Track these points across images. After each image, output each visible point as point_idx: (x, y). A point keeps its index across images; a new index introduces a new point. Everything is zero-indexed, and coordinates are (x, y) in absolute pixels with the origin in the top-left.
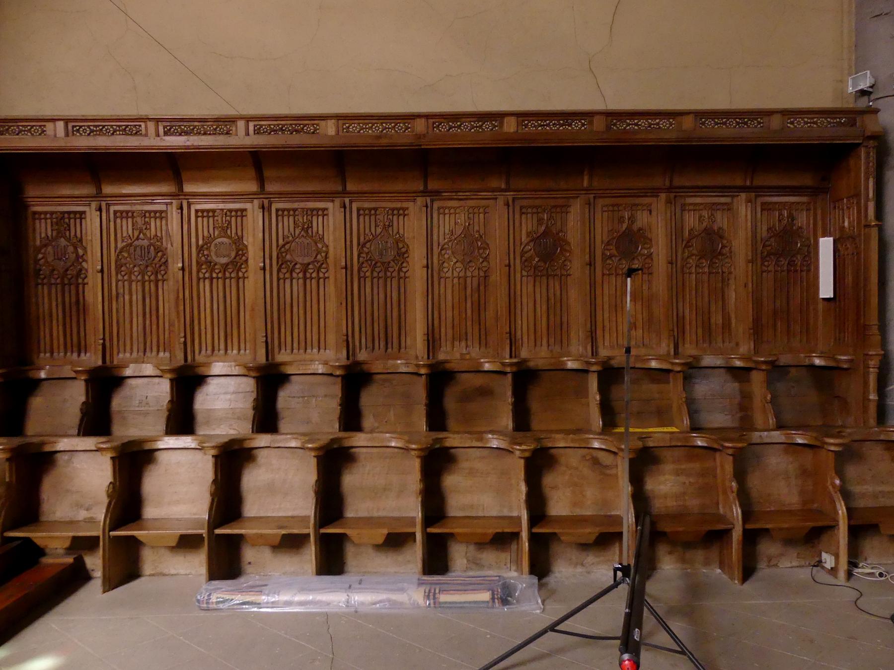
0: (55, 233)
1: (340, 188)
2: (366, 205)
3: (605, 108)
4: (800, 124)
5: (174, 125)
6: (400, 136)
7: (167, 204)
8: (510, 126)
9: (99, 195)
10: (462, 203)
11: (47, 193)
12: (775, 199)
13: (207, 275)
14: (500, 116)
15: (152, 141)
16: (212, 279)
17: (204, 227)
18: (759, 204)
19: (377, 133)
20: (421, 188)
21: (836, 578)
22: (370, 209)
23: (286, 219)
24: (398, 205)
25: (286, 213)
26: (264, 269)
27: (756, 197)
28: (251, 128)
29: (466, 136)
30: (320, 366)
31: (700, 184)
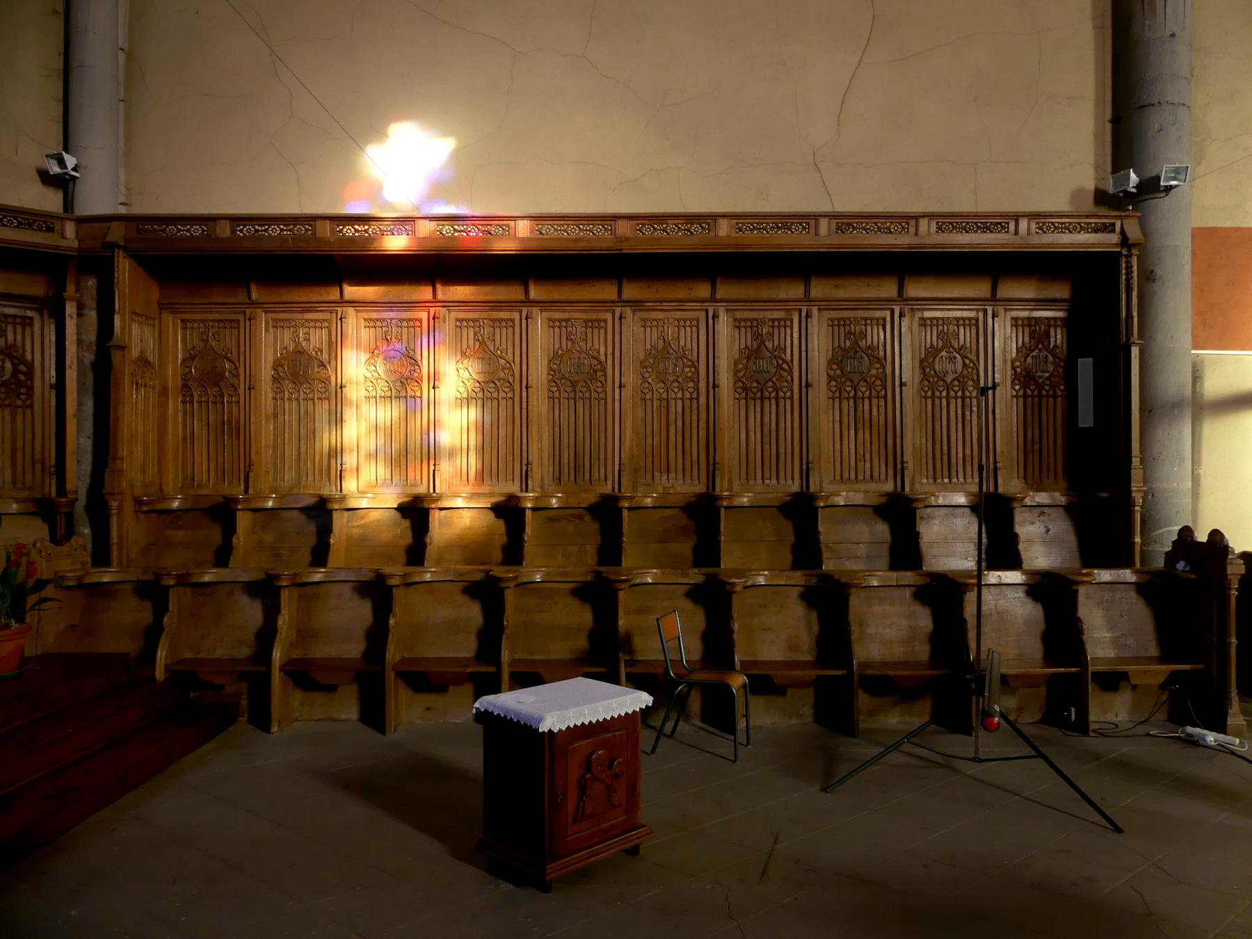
0: (940, 343)
1: (522, 297)
2: (557, 315)
3: (831, 210)
4: (623, 228)
5: (949, 221)
6: (600, 238)
7: (978, 310)
8: (724, 229)
9: (901, 297)
10: (667, 314)
11: (288, 298)
12: (938, 314)
13: (1051, 392)
14: (714, 217)
15: (929, 236)
16: (762, 399)
17: (931, 337)
18: (1008, 318)
19: (573, 236)
20: (988, 295)
21: (383, 733)
22: (560, 321)
23: (782, 329)
24: (594, 316)
25: (688, 323)
26: (807, 386)
27: (1006, 310)
28: (834, 226)
29: (676, 241)
30: (14, 506)
31: (939, 295)
